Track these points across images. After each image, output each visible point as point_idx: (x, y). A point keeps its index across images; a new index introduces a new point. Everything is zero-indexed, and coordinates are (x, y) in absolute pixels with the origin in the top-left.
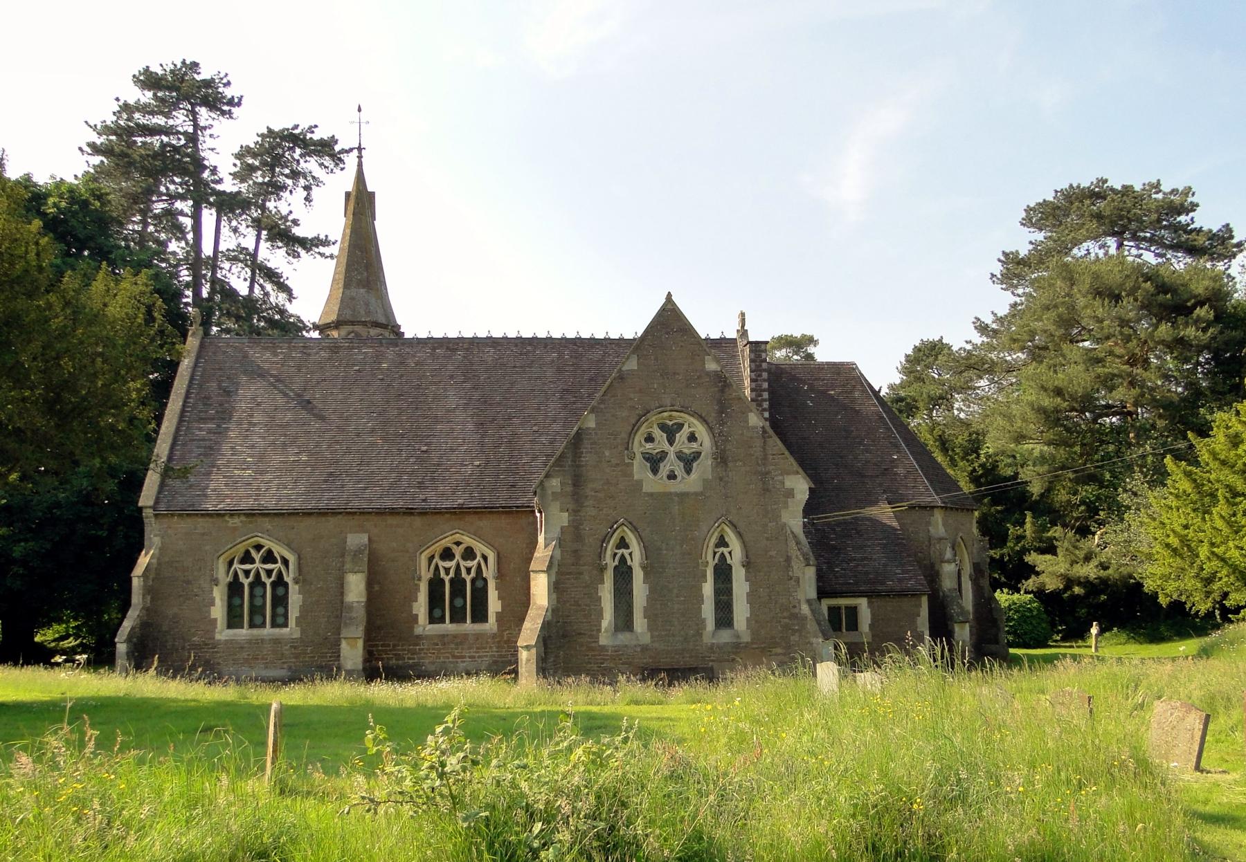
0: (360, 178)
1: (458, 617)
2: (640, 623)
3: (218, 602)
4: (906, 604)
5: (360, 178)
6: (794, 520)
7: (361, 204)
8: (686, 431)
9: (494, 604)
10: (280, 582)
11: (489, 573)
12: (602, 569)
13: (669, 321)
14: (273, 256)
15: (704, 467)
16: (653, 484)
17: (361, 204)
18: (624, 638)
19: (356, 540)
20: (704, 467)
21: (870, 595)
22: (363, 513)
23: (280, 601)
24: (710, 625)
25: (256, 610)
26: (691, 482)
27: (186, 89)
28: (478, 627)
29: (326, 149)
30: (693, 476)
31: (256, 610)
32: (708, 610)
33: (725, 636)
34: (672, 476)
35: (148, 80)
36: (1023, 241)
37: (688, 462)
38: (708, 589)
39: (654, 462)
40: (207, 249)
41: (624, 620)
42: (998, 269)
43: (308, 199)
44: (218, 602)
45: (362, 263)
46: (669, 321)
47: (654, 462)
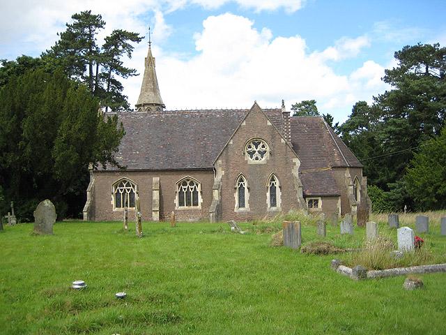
0: (150, 53)
1: (188, 204)
2: (247, 205)
3: (113, 199)
4: (334, 200)
5: (150, 53)
6: (296, 173)
7: (150, 61)
8: (261, 144)
9: (200, 200)
10: (132, 193)
11: (199, 189)
12: (236, 188)
13: (255, 106)
14: (118, 78)
15: (267, 156)
16: (251, 161)
17: (150, 61)
18: (242, 209)
19: (156, 179)
20: (267, 156)
21: (323, 197)
22: (157, 171)
23: (196, 198)
24: (269, 206)
25: (188, 199)
26: (263, 160)
27: (88, 20)
28: (195, 207)
29: (134, 37)
30: (264, 159)
31: (188, 199)
32: (268, 201)
33: (274, 208)
34: (257, 159)
35: (75, 17)
36: (395, 64)
37: (262, 153)
38: (268, 194)
39: (251, 154)
40: (95, 74)
41: (242, 204)
42: (384, 75)
43: (130, 57)
44: (113, 199)
45: (151, 81)
46: (255, 106)
47: (251, 154)
